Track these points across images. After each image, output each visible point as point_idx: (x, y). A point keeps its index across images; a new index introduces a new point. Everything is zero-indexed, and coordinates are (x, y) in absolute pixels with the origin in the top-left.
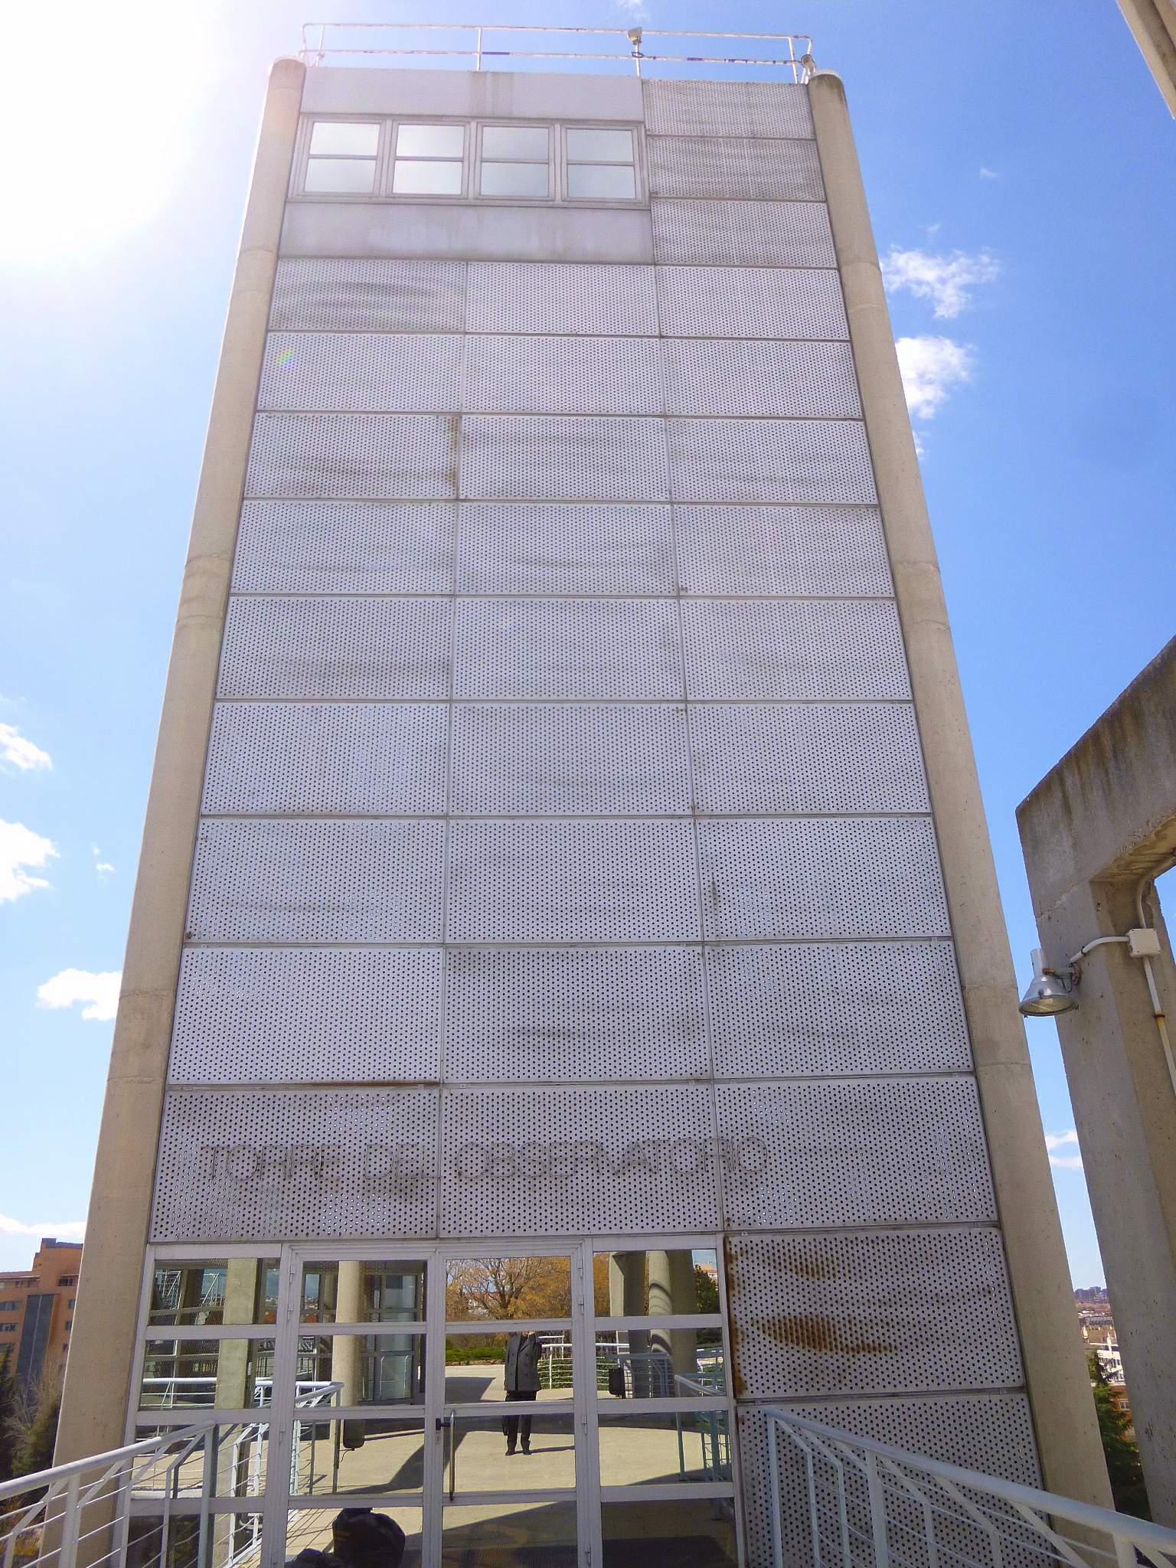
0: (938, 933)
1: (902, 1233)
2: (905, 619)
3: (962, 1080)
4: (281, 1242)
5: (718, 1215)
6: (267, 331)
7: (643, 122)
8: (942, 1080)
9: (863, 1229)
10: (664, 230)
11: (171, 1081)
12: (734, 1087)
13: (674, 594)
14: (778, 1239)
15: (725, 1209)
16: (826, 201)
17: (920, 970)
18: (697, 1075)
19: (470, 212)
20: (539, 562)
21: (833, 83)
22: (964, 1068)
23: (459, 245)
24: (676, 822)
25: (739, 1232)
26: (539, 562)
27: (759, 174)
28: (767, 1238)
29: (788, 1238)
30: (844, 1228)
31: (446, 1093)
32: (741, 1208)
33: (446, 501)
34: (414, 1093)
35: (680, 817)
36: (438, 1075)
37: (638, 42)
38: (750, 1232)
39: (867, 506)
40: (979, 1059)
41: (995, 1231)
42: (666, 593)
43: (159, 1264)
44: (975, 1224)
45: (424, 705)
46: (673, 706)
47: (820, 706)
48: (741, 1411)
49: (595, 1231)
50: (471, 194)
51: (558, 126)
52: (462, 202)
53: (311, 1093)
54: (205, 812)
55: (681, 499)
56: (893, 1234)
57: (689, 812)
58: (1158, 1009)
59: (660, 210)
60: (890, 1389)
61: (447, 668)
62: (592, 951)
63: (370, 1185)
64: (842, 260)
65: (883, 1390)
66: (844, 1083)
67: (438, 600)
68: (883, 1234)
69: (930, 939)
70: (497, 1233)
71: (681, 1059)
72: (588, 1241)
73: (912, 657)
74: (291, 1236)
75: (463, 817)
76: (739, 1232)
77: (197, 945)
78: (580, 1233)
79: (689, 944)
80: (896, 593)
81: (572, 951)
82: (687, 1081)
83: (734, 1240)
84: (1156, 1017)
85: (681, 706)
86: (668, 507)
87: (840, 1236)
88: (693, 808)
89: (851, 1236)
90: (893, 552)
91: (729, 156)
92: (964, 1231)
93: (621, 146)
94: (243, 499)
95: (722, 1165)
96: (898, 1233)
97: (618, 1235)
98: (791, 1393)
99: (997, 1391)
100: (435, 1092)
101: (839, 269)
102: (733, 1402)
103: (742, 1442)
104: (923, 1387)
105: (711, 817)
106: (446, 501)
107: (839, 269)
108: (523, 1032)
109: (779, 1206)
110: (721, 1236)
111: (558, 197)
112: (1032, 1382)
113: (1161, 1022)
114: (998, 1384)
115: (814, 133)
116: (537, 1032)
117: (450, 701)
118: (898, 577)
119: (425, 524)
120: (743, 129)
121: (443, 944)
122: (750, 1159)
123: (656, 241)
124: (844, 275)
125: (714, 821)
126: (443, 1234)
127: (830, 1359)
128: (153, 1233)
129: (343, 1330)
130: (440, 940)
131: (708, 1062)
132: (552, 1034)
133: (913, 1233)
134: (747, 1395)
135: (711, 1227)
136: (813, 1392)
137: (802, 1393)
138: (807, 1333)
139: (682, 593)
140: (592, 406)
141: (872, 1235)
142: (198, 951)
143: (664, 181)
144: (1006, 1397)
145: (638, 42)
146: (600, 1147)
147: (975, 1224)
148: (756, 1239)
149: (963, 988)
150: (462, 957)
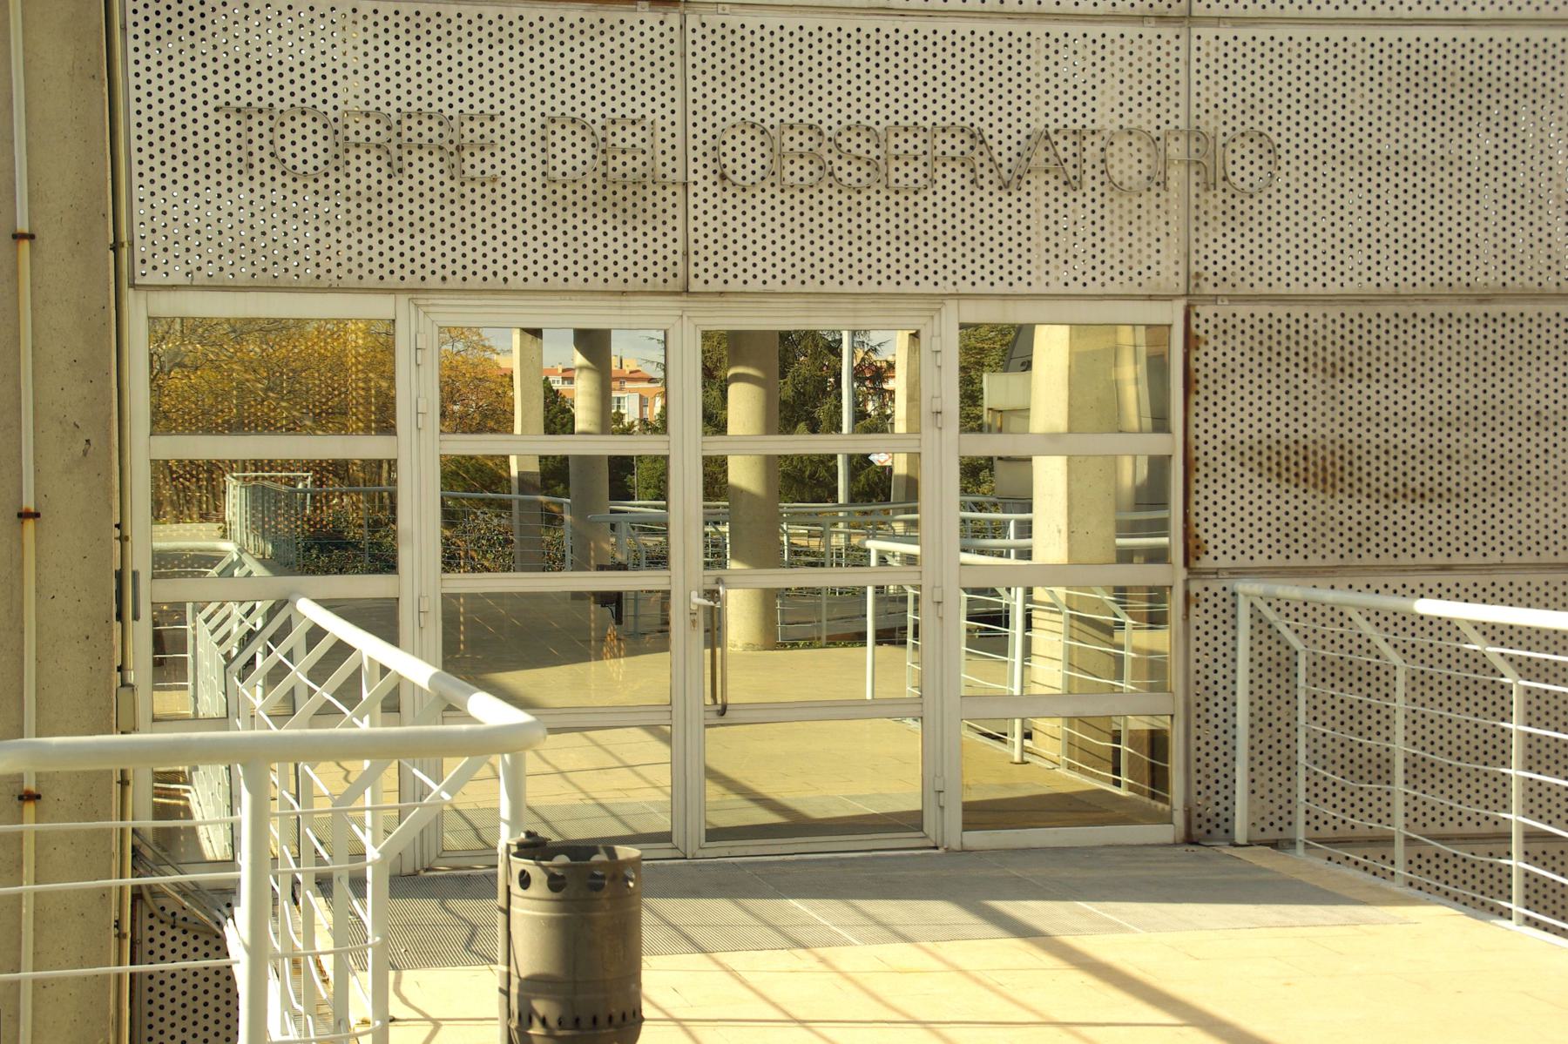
1: (1494, 310)
9: (1426, 299)
14: (1280, 311)
25: (1215, 299)
28: (1262, 310)
29: (1298, 311)
32: (1221, 252)
38: (1234, 299)
48: (1196, 587)
49: (964, 287)
56: (1478, 310)
60: (1440, 559)
68: (1460, 310)
72: (951, 305)
76: (1215, 299)
82: (1142, 18)
83: (1206, 311)
87: (1388, 311)
96: (1484, 308)
98: (1279, 560)
102: (1182, 573)
104: (1494, 558)
110: (1179, 306)
122: (1244, 166)
134: (1206, 562)
136: (1314, 561)
137: (1296, 561)
138: (1312, 468)
148: (1243, 311)
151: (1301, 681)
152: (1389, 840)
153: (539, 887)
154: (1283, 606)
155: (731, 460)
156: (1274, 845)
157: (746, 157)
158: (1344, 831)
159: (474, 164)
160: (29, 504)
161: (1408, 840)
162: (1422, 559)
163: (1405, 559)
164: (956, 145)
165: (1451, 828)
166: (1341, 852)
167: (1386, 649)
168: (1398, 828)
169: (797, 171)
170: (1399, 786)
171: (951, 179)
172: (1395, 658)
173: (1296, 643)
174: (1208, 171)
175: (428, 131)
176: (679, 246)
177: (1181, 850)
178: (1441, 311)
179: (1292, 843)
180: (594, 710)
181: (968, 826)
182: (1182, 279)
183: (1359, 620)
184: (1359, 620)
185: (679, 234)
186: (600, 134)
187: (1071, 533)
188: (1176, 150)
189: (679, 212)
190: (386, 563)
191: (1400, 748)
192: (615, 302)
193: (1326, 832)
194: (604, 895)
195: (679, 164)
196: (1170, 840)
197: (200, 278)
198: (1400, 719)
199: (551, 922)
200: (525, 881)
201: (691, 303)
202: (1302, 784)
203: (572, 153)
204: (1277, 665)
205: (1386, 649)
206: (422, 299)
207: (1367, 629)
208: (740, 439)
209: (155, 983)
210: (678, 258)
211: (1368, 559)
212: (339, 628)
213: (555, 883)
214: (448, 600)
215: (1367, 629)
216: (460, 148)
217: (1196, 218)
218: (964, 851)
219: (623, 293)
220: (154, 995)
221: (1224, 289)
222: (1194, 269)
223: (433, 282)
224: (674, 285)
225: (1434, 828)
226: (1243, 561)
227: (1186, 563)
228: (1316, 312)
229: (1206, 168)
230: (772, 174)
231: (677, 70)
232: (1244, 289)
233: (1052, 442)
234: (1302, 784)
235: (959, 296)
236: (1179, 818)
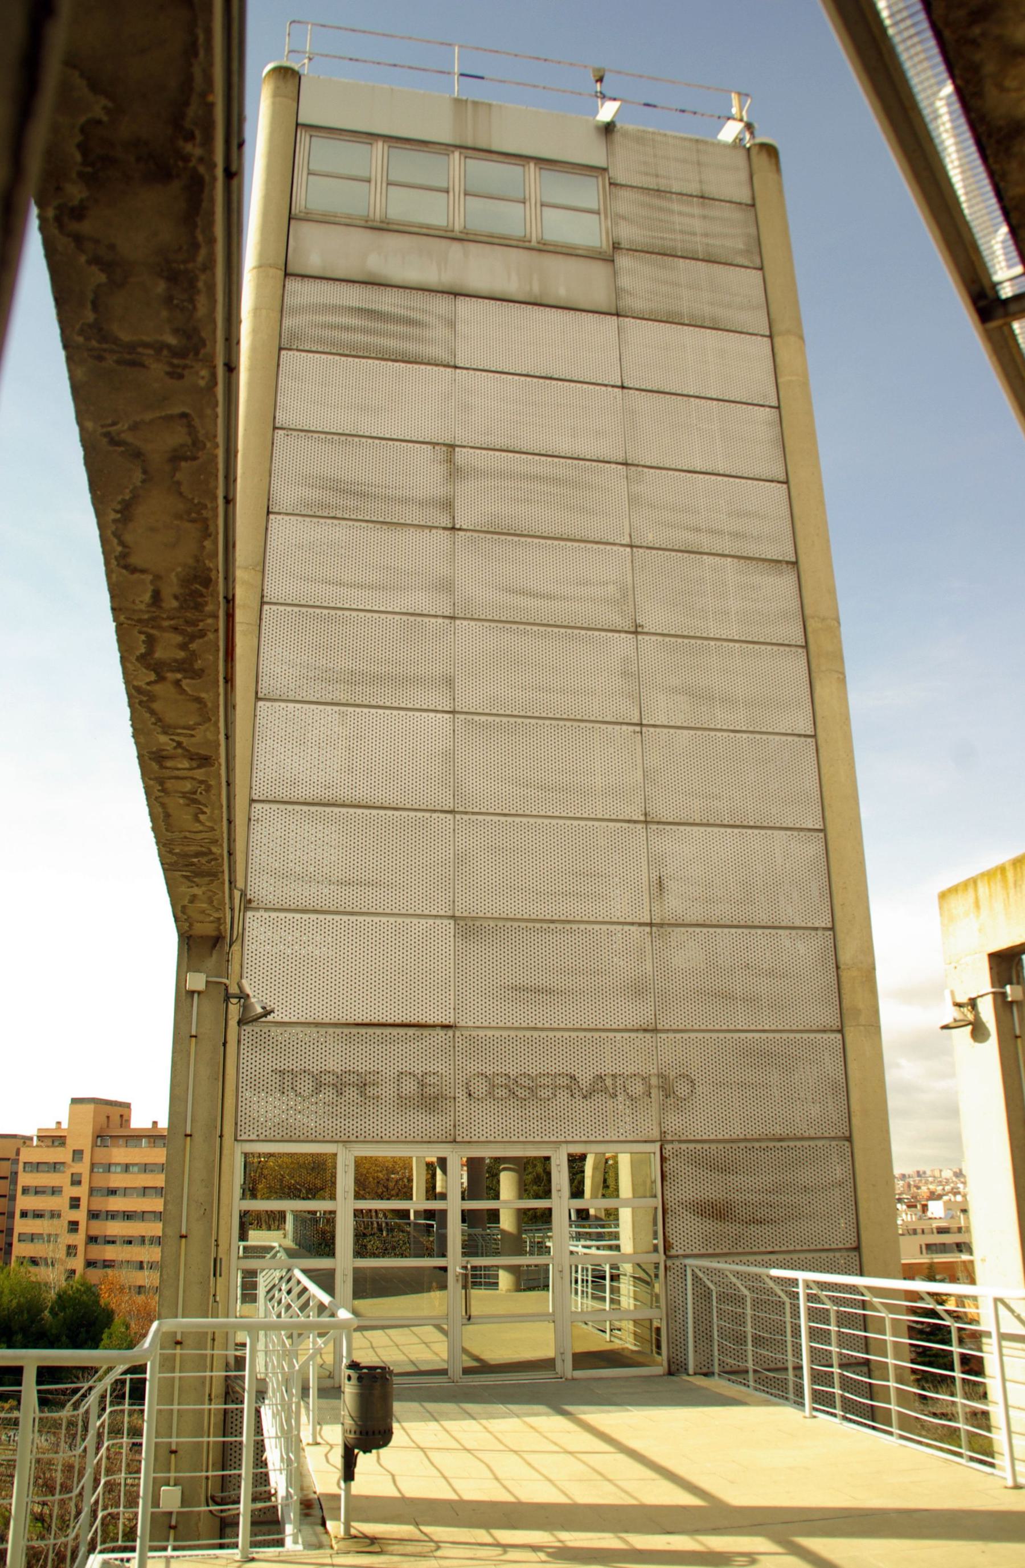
0: (823, 925)
1: (784, 1144)
2: (813, 666)
3: (833, 1036)
6: (280, 349)
7: (605, 170)
8: (819, 1036)
9: (757, 1140)
10: (625, 281)
13: (633, 629)
14: (699, 1146)
16: (761, 269)
17: (804, 952)
18: (645, 1026)
19: (456, 246)
20: (523, 593)
21: (770, 151)
22: (835, 1028)
23: (446, 278)
24: (632, 826)
25: (672, 1142)
26: (523, 593)
27: (706, 235)
28: (691, 1146)
29: (706, 1146)
31: (458, 1034)
32: (674, 1123)
33: (445, 528)
34: (433, 1033)
35: (635, 822)
36: (452, 1020)
37: (600, 80)
38: (680, 1141)
39: (787, 563)
40: (846, 1021)
41: (847, 1144)
42: (626, 629)
44: (834, 1138)
45: (432, 715)
46: (631, 728)
47: (745, 736)
48: (669, 1263)
49: (569, 1138)
50: (457, 228)
51: (532, 165)
52: (449, 234)
53: (354, 1031)
54: (277, 425)
55: (638, 544)
56: (778, 1144)
57: (642, 818)
58: (1018, 1032)
59: (623, 261)
60: (770, 1249)
61: (450, 682)
62: (568, 926)
63: (402, 1101)
64: (774, 329)
66: (750, 1035)
67: (440, 620)
68: (771, 1144)
69: (816, 929)
70: (499, 1139)
71: (636, 1013)
72: (564, 1145)
73: (817, 700)
75: (466, 813)
76: (672, 1142)
77: (257, 909)
79: (640, 924)
80: (806, 642)
81: (552, 926)
82: (637, 1030)
83: (668, 1147)
84: (1017, 1037)
85: (638, 729)
86: (628, 549)
87: (742, 1145)
88: (646, 815)
90: (806, 607)
91: (680, 214)
92: (826, 1143)
93: (588, 193)
94: (262, 603)
96: (781, 1144)
97: (586, 1142)
98: (703, 1251)
99: (840, 1250)
100: (450, 1033)
101: (771, 336)
102: (663, 1257)
103: (669, 1283)
104: (791, 1248)
105: (658, 823)
106: (445, 528)
107: (771, 336)
108: (516, 988)
110: (658, 1145)
111: (534, 239)
112: (864, 1244)
113: (1019, 1041)
114: (841, 1246)
115: (753, 198)
116: (526, 989)
117: (453, 712)
118: (809, 629)
119: (428, 549)
120: (693, 188)
121: (453, 917)
122: (682, 1089)
123: (618, 292)
124: (776, 345)
125: (661, 827)
126: (459, 1139)
128: (239, 1133)
130: (450, 913)
132: (538, 990)
133: (792, 1144)
134: (673, 1252)
136: (718, 1251)
137: (711, 1251)
138: (716, 1211)
139: (639, 629)
140: (564, 448)
142: (258, 914)
143: (627, 233)
144: (845, 1254)
145: (600, 80)
146: (573, 1078)
147: (834, 1138)
148: (684, 1146)
149: (838, 968)
150: (467, 927)
151: (714, 1303)
152: (747, 1372)
153: (354, 1381)
154: (707, 1271)
155: (502, 1211)
156: (705, 1375)
157: (480, 1088)
158: (735, 1368)
159: (370, 1091)
160: (184, 1232)
161: (755, 1371)
162: (762, 1249)
163: (755, 1249)
164: (566, 1081)
165: (772, 1366)
166: (733, 1377)
167: (742, 1288)
168: (750, 1365)
169: (502, 1092)
170: (750, 1347)
171: (563, 1095)
172: (746, 1292)
173: (712, 1287)
174: (667, 1090)
175: (354, 1078)
176: (452, 1123)
177: (666, 1377)
178: (764, 1145)
179: (713, 1374)
180: (408, 1318)
181: (575, 1368)
182: (658, 1134)
183: (731, 1276)
184: (731, 1276)
185: (452, 1118)
186: (421, 1078)
187: (634, 1239)
188: (654, 1081)
189: (452, 1109)
190: (331, 1254)
191: (749, 1329)
192: (425, 1146)
193: (728, 1368)
194: (378, 1384)
195: (452, 1090)
196: (661, 1373)
197: (262, 1137)
198: (749, 1320)
199: (357, 1394)
200: (349, 1378)
201: (457, 1146)
202: (716, 1348)
203: (410, 1087)
204: (704, 1295)
205: (742, 1288)
206: (348, 1145)
207: (734, 1280)
208: (505, 1202)
209: (233, 1447)
210: (452, 1128)
211: (740, 1250)
212: (306, 1282)
213: (360, 1379)
214: (356, 1270)
215: (734, 1280)
216: (365, 1085)
217: (663, 1109)
218: (573, 1379)
219: (469, 1142)
220: (232, 1452)
221: (676, 1138)
222: (663, 1130)
223: (353, 1138)
224: (450, 1139)
225: (766, 1366)
226: (689, 1252)
227: (665, 1253)
228: (713, 1146)
229: (667, 1088)
230: (490, 1093)
231: (452, 1053)
232: (684, 1138)
233: (626, 1203)
234: (716, 1348)
235: (567, 1142)
236: (665, 1363)
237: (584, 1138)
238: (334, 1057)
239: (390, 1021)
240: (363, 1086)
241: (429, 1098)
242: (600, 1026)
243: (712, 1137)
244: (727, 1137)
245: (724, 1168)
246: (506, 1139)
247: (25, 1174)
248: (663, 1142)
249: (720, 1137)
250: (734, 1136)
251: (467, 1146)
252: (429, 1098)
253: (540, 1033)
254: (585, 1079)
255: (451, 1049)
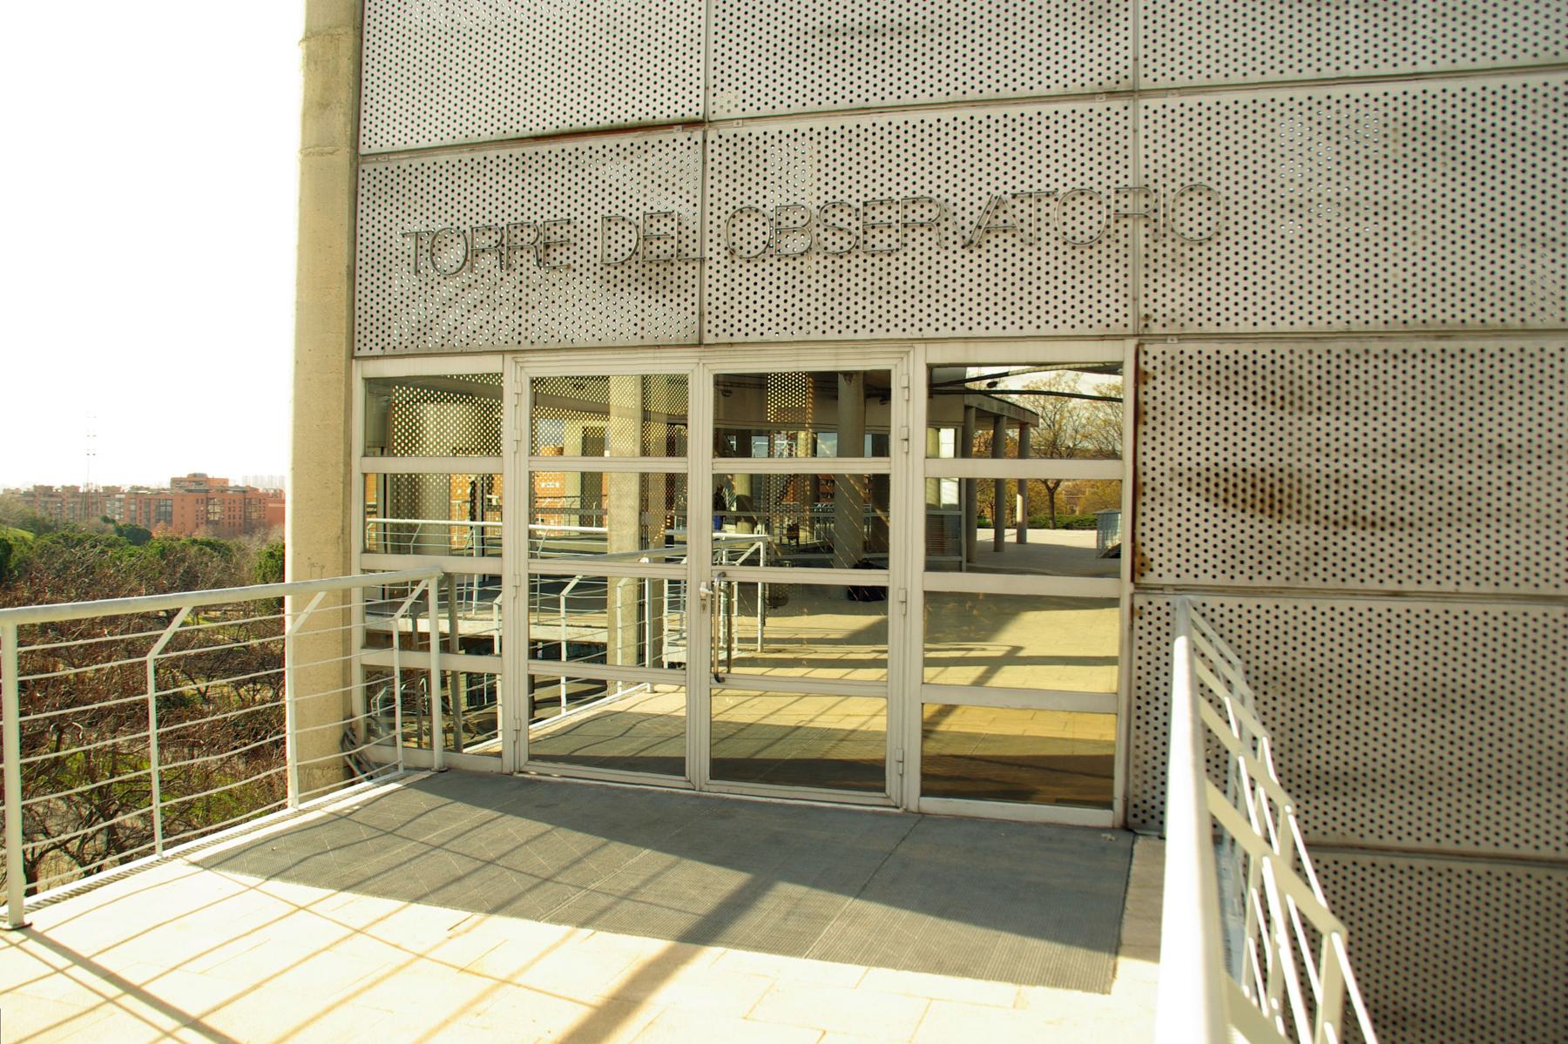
1: (1452, 346)
4: (502, 352)
5: (1129, 311)
11: (363, 150)
12: (1173, 101)
14: (1228, 348)
15: (1143, 301)
25: (1163, 338)
28: (1209, 348)
30: (1348, 334)
31: (712, 135)
32: (1172, 297)
36: (701, 110)
38: (1182, 337)
43: (370, 382)
49: (929, 333)
53: (530, 150)
56: (1435, 346)
65: (1378, 587)
72: (920, 348)
74: (513, 345)
76: (1163, 338)
78: (906, 335)
83: (1154, 349)
89: (1357, 347)
95: (1143, 231)
97: (966, 339)
98: (1223, 580)
100: (697, 135)
104: (1449, 586)
108: (828, 32)
109: (1254, 292)
110: (1131, 344)
122: (1191, 219)
127: (1296, 535)
129: (292, 589)
131: (1130, 62)
132: (876, 32)
133: (1472, 346)
134: (1150, 578)
135: (1117, 329)
137: (1241, 581)
138: (1263, 495)
141: (1395, 347)
148: (1190, 348)
159: (557, 256)
162: (1372, 585)
178: (1395, 347)
206: (521, 357)
211: (1315, 583)
232: (1192, 328)
237: (962, 332)
238: (504, 198)
239: (591, 125)
240: (545, 249)
241: (654, 261)
242: (1006, 93)
243: (1264, 327)
244: (1300, 326)
245: (1283, 396)
246: (798, 336)
247: (276, 485)
248: (1142, 338)
249: (1283, 326)
250: (1320, 326)
251: (726, 351)
252: (654, 261)
253: (875, 118)
254: (969, 202)
255: (706, 309)
